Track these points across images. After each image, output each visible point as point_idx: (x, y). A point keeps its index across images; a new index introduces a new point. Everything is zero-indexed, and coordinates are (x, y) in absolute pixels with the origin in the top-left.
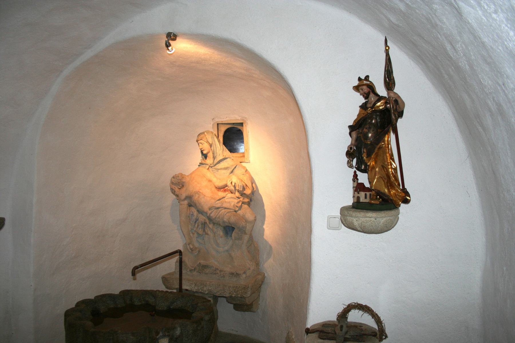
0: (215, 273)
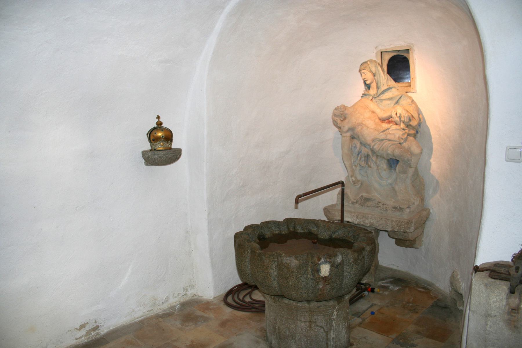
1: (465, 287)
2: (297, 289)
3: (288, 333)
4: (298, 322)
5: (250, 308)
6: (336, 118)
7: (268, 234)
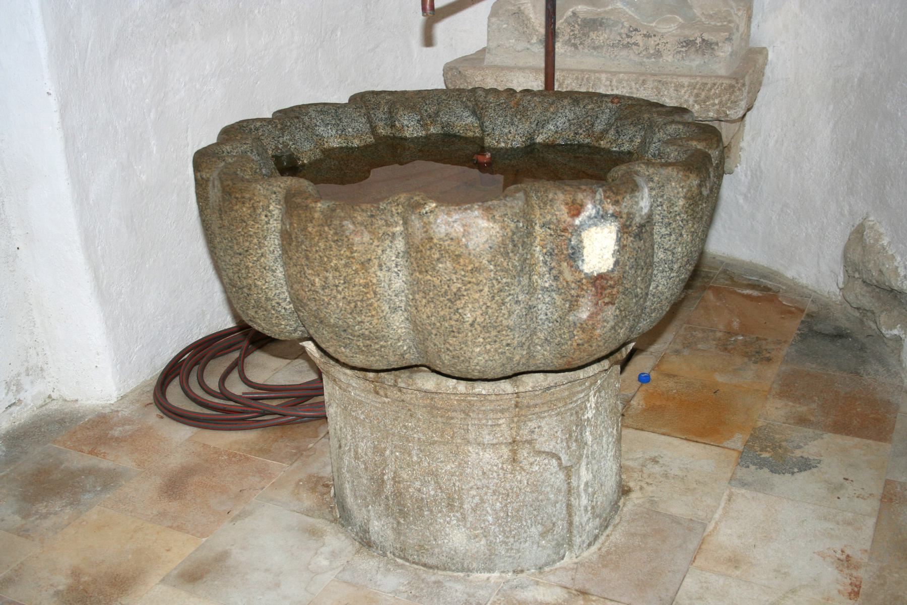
0: (628, 43)
2: (494, 333)
3: (432, 493)
4: (470, 449)
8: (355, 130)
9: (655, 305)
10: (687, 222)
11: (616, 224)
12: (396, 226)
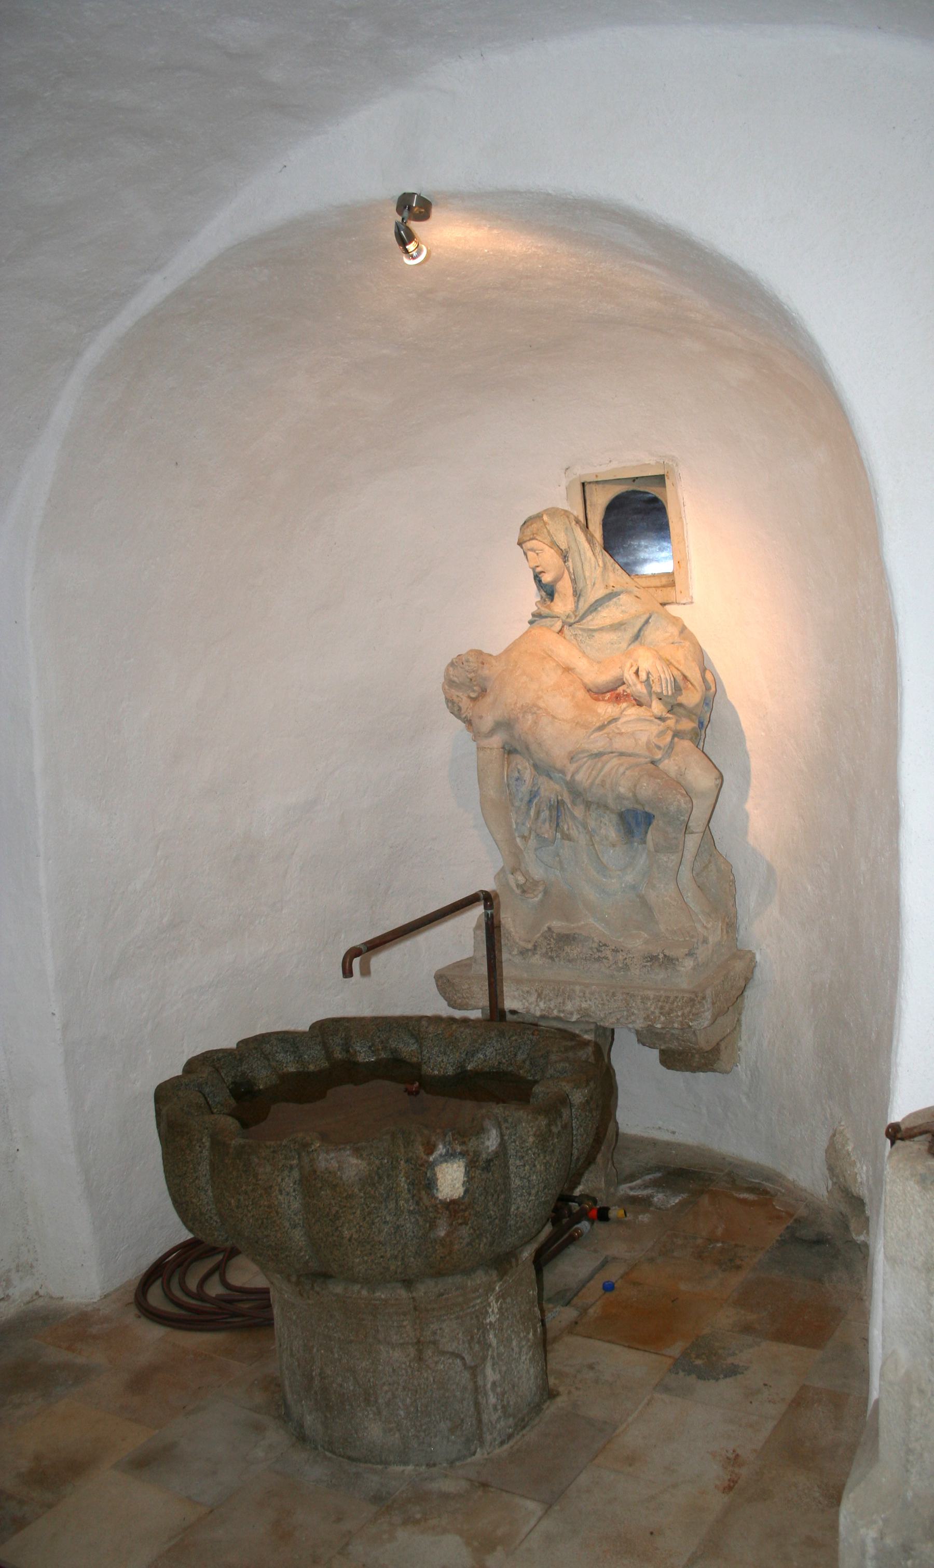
0: (599, 957)
1: (868, 1178)
2: (368, 1247)
3: (351, 1388)
4: (382, 1347)
5: (224, 1316)
6: (454, 693)
7: (263, 1077)
8: (311, 1057)
9: (519, 1223)
10: (539, 1155)
11: (464, 1160)
12: (293, 1160)
